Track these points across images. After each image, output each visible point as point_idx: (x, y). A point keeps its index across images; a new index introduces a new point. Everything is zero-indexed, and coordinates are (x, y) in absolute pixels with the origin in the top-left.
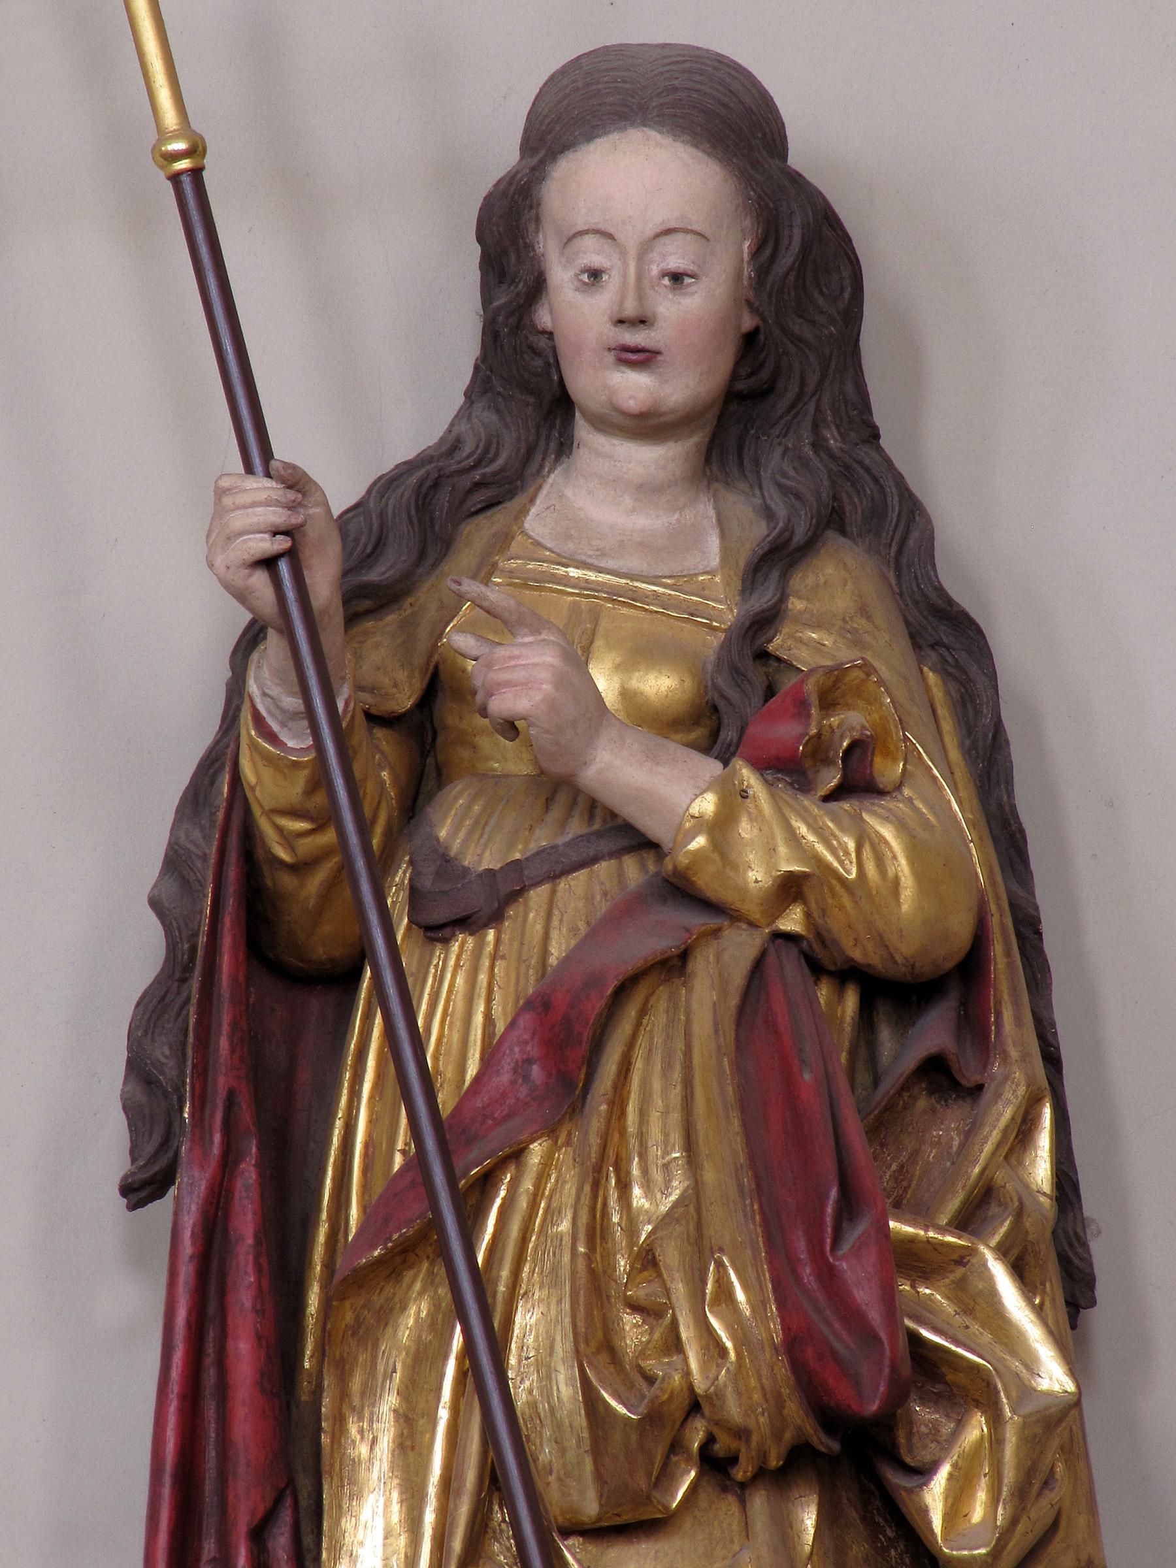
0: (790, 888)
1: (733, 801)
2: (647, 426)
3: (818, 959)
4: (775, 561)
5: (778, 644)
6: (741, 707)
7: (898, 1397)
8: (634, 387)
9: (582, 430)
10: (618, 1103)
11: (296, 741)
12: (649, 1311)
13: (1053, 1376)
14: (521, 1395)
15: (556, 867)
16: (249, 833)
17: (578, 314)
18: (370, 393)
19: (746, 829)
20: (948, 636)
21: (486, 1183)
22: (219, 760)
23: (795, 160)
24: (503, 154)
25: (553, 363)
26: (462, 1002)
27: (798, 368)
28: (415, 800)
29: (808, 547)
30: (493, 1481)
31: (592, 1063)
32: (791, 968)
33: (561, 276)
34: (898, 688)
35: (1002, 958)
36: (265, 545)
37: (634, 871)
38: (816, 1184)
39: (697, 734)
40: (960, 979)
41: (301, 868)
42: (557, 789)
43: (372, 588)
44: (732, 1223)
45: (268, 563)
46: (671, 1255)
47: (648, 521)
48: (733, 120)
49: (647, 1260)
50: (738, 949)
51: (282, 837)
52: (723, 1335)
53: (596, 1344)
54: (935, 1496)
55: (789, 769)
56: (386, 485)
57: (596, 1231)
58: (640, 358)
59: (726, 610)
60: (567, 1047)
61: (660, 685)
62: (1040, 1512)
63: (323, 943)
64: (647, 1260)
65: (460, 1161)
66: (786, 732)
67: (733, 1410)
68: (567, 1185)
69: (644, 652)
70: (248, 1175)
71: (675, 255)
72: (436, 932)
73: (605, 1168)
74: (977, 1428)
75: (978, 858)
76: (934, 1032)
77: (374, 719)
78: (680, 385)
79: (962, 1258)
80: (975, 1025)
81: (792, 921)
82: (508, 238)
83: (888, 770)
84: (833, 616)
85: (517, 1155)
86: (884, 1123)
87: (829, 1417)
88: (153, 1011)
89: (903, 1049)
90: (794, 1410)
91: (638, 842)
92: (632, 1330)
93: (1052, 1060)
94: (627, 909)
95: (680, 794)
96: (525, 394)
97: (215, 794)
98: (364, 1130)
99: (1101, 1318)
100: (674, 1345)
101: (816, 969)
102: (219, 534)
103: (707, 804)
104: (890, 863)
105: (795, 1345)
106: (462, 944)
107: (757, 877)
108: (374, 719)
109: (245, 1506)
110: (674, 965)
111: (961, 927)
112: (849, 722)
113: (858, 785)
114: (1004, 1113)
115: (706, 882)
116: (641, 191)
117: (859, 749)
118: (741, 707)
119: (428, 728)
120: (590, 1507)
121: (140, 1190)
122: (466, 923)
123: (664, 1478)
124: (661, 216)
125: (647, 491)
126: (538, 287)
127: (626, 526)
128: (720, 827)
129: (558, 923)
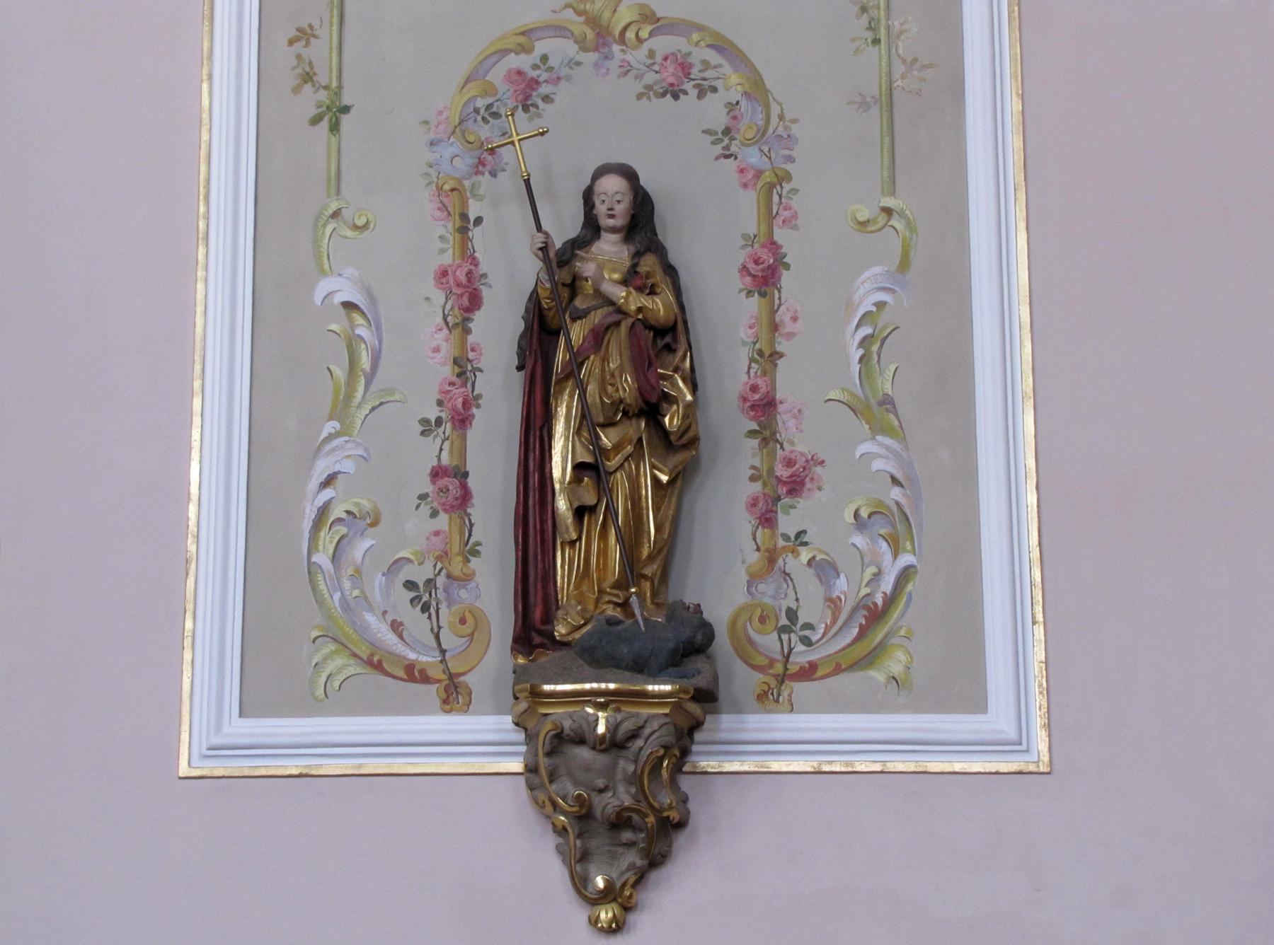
0: (640, 310)
1: (629, 294)
2: (613, 230)
3: (647, 325)
4: (637, 255)
5: (638, 269)
6: (631, 278)
7: (659, 401)
8: (611, 222)
9: (602, 233)
10: (607, 348)
11: (548, 285)
12: (612, 385)
13: (689, 398)
14: (589, 401)
15: (596, 308)
16: (540, 303)
17: (601, 209)
18: (563, 224)
19: (631, 299)
20: (671, 271)
21: (582, 364)
22: (535, 292)
23: (642, 183)
24: (588, 182)
25: (597, 221)
26: (578, 332)
27: (641, 221)
28: (573, 296)
29: (644, 253)
30: (583, 416)
31: (603, 339)
32: (639, 327)
33: (597, 203)
34: (659, 277)
35: (680, 326)
36: (541, 245)
37: (611, 309)
38: (643, 363)
39: (645, 408)
40: (672, 329)
41: (550, 309)
42: (598, 293)
43: (561, 261)
44: (628, 367)
45: (541, 249)
46: (617, 374)
47: (614, 249)
48: (629, 174)
49: (613, 376)
50: (630, 321)
51: (545, 303)
52: (627, 386)
53: (603, 390)
54: (667, 420)
55: (640, 289)
56: (565, 244)
57: (603, 370)
58: (612, 216)
59: (628, 264)
60: (598, 338)
61: (616, 276)
62: (687, 422)
63: (554, 326)
64: (613, 376)
65: (577, 360)
66: (639, 283)
67: (628, 401)
68: (598, 363)
69: (614, 270)
70: (539, 364)
71: (618, 197)
72: (574, 320)
73: (605, 360)
74: (675, 407)
75: (676, 309)
76: (668, 339)
77: (564, 285)
78: (619, 222)
79: (672, 377)
80: (675, 339)
81: (640, 316)
82: (588, 197)
83: (658, 290)
84: (649, 263)
85: (588, 358)
86: (658, 355)
87: (646, 402)
88: (522, 337)
89: (660, 343)
90: (640, 401)
91: (612, 303)
92: (610, 389)
93: (690, 347)
94: (609, 314)
95: (619, 293)
96: (592, 228)
97: (534, 298)
98: (561, 356)
99: (699, 393)
100: (617, 390)
101: (646, 327)
102: (533, 244)
103: (624, 294)
104: (660, 306)
105: (639, 388)
106: (579, 322)
107: (633, 308)
108: (564, 285)
109: (539, 423)
110: (617, 324)
111: (672, 318)
112: (650, 282)
113: (652, 292)
114: (680, 353)
115: (624, 308)
116: (612, 185)
117: (653, 286)
118: (631, 278)
119: (573, 286)
120: (601, 420)
121: (520, 368)
122: (580, 318)
123: (615, 414)
124: (615, 189)
125: (615, 243)
126: (593, 206)
127: (610, 251)
128: (626, 298)
129: (597, 317)
